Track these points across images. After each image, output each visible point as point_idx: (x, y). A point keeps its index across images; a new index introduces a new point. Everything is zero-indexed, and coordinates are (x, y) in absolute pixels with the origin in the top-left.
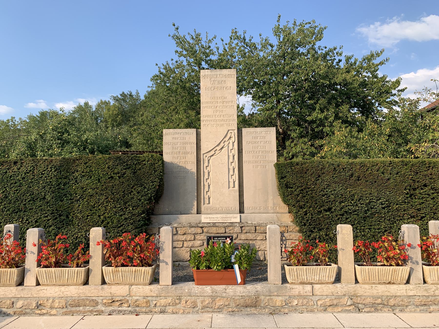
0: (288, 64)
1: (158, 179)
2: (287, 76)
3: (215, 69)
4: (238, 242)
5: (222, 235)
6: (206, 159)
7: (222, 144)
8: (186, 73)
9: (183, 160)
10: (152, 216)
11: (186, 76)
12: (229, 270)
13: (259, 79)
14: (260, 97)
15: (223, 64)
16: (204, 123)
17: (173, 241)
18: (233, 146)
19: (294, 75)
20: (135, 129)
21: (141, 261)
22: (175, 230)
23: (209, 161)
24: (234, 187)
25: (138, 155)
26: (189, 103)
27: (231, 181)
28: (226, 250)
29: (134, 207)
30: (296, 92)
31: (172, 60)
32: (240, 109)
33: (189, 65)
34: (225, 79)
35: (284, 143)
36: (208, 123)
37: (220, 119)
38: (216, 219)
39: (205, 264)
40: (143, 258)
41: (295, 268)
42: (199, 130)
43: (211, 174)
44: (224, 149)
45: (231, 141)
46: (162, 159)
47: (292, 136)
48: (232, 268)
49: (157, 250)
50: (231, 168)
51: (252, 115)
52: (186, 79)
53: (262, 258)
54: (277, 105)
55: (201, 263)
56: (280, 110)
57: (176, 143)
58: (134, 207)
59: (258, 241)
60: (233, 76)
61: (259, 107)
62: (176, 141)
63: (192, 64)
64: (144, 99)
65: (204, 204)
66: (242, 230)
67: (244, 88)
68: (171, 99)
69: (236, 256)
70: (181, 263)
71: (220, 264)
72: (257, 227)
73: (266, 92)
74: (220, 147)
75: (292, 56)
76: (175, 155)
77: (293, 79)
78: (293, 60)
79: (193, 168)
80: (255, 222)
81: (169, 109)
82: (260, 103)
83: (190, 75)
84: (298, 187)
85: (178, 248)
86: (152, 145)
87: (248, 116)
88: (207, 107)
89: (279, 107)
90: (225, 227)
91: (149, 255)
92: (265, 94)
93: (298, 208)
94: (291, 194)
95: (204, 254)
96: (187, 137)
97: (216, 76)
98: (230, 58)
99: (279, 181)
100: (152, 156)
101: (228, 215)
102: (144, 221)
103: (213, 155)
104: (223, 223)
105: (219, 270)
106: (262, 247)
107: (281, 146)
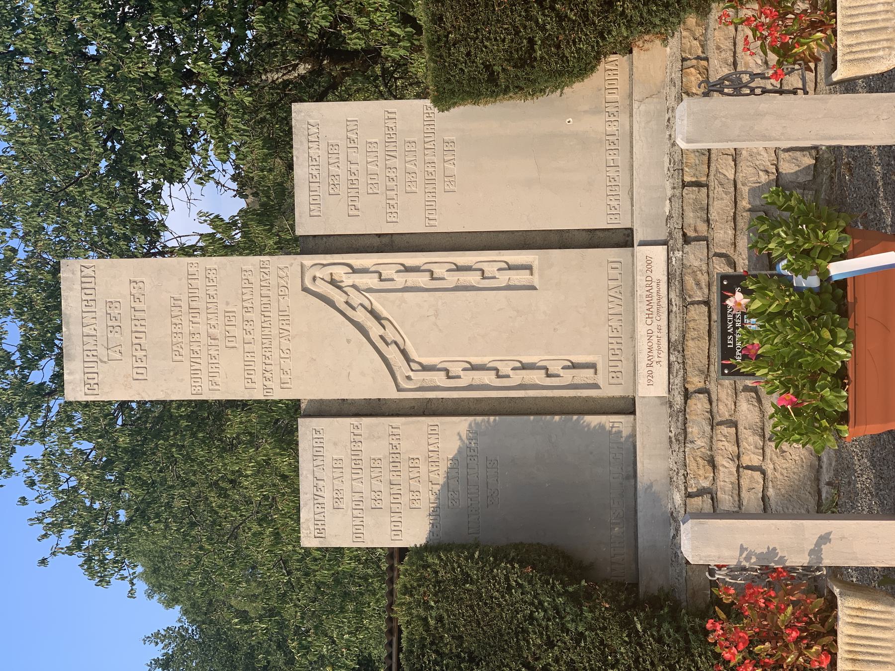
0: (38, 41)
1: (497, 566)
2: (86, 42)
3: (59, 329)
4: (745, 254)
5: (715, 317)
6: (420, 378)
7: (361, 316)
8: (75, 445)
9: (423, 468)
10: (642, 590)
11: (86, 446)
12: (850, 298)
13: (100, 156)
14: (170, 153)
15: (38, 298)
16: (274, 385)
17: (738, 513)
18: (365, 271)
19: (83, 18)
20: (302, 647)
21: (815, 637)
22: (697, 502)
23: (425, 368)
24: (529, 268)
25: (404, 644)
26: (194, 435)
27: (504, 278)
28: (773, 308)
29: (605, 661)
30: (152, 8)
31: (23, 501)
32: (221, 241)
33: (43, 435)
35: (356, 52)
36: (275, 369)
37: (258, 325)
38: (655, 339)
39: (827, 393)
40: (802, 630)
41: (842, 40)
42: (303, 406)
43: (476, 360)
45: (348, 280)
46: (419, 551)
47: (324, 23)
48: (842, 284)
49: (772, 576)
50: (452, 279)
51: (243, 183)
52: (99, 447)
53: (809, 161)
54: (200, 85)
55: (821, 405)
56: (221, 73)
57: (357, 497)
58: (605, 661)
59: (740, 175)
60: (87, 272)
61: (211, 153)
62: (347, 495)
63: (40, 422)
64: (178, 608)
65: (596, 386)
66: (698, 239)
67: (133, 213)
68: (178, 504)
69: (796, 272)
70: (826, 477)
71: (826, 334)
72: (687, 179)
73: (151, 127)
74: (370, 325)
75: (8, 23)
76: (405, 499)
77: (97, 22)
78: (20, 19)
79: (453, 432)
80: (668, 185)
81: (222, 513)
82: (193, 152)
83: (85, 429)
84: (529, 18)
85: (765, 488)
86: (365, 578)
87: (245, 197)
88: (212, 377)
89: (212, 75)
90: (686, 305)
91: (790, 609)
92: (157, 131)
93: (611, 17)
94: (558, 47)
95: (789, 396)
96: (330, 453)
97: (91, 340)
98: (14, 272)
99: (506, 91)
100: (407, 591)
101: (641, 291)
102: (661, 620)
103: (404, 352)
104: (669, 312)
105: (851, 337)
106: (766, 160)
107: (366, 66)
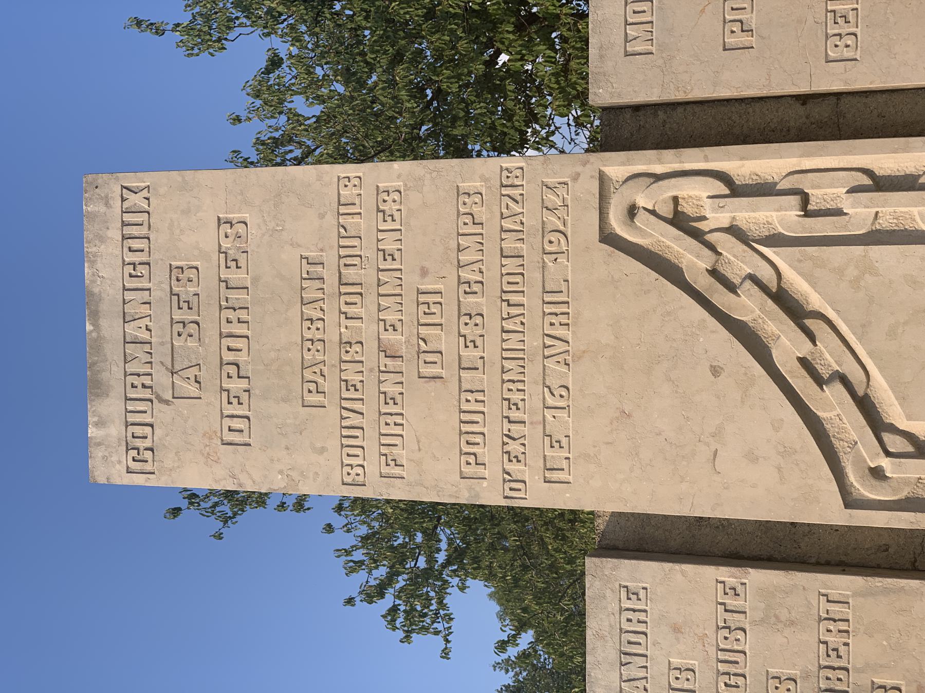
7: (750, 306)
18: (763, 190)
31: (329, 528)
34: (160, 274)
36: (532, 433)
37: (493, 324)
44: (798, 284)
45: (717, 217)
60: (135, 200)
74: (767, 330)
96: (664, 652)
103: (866, 407)
